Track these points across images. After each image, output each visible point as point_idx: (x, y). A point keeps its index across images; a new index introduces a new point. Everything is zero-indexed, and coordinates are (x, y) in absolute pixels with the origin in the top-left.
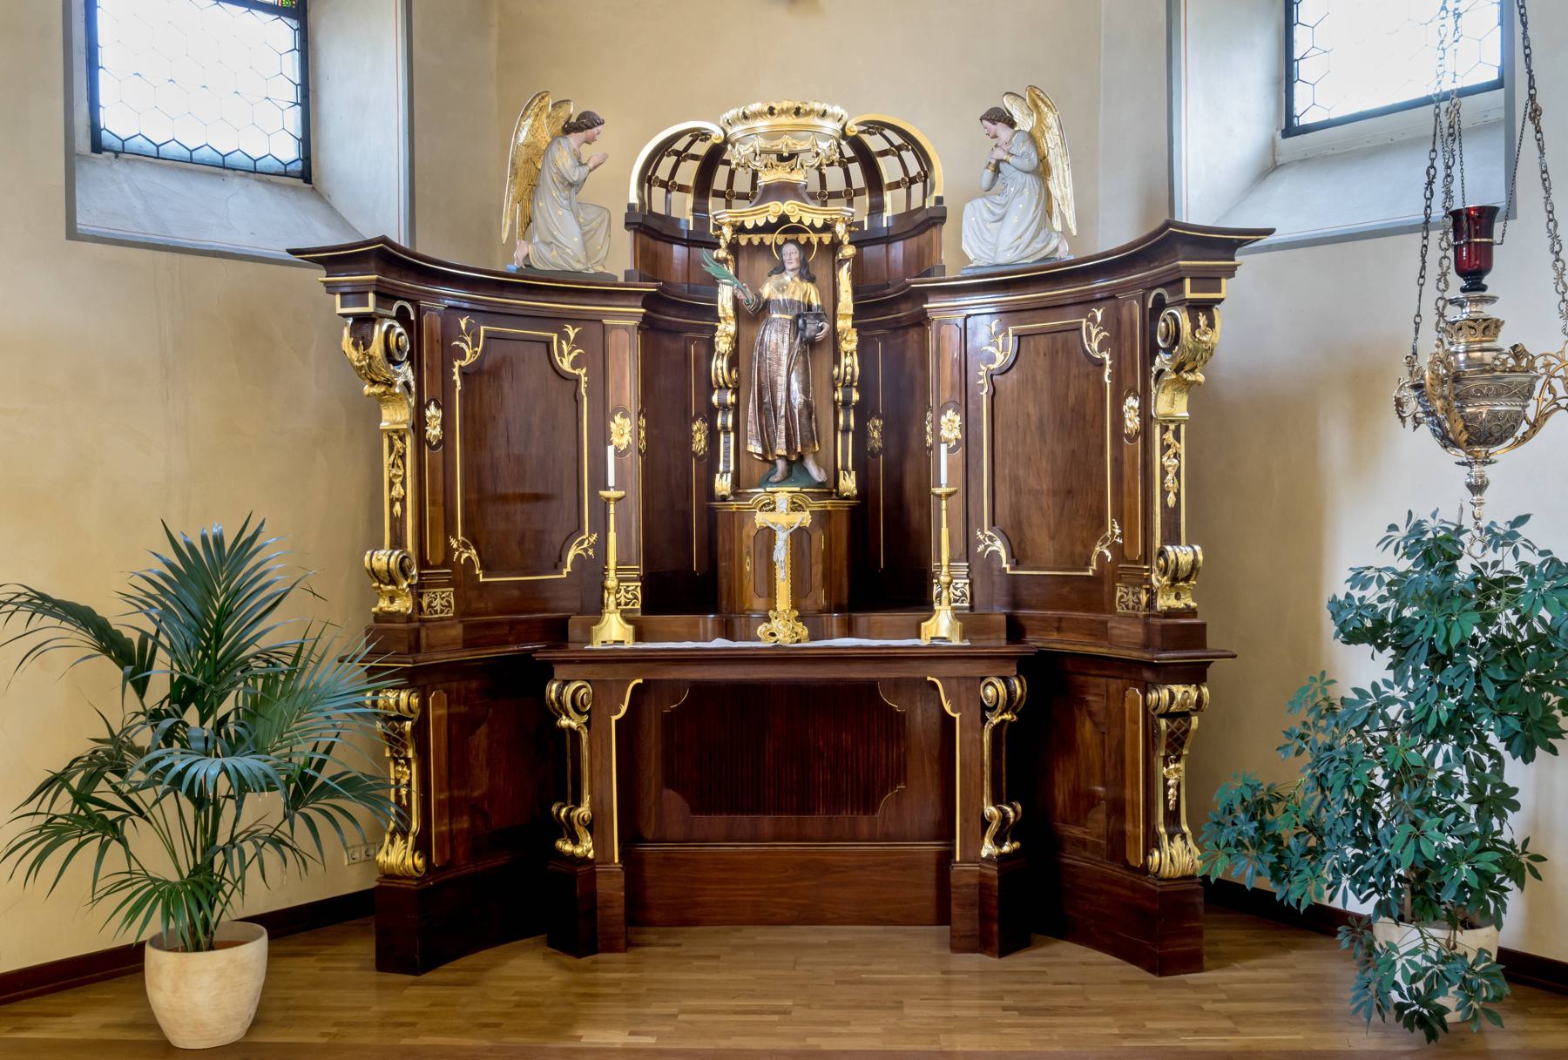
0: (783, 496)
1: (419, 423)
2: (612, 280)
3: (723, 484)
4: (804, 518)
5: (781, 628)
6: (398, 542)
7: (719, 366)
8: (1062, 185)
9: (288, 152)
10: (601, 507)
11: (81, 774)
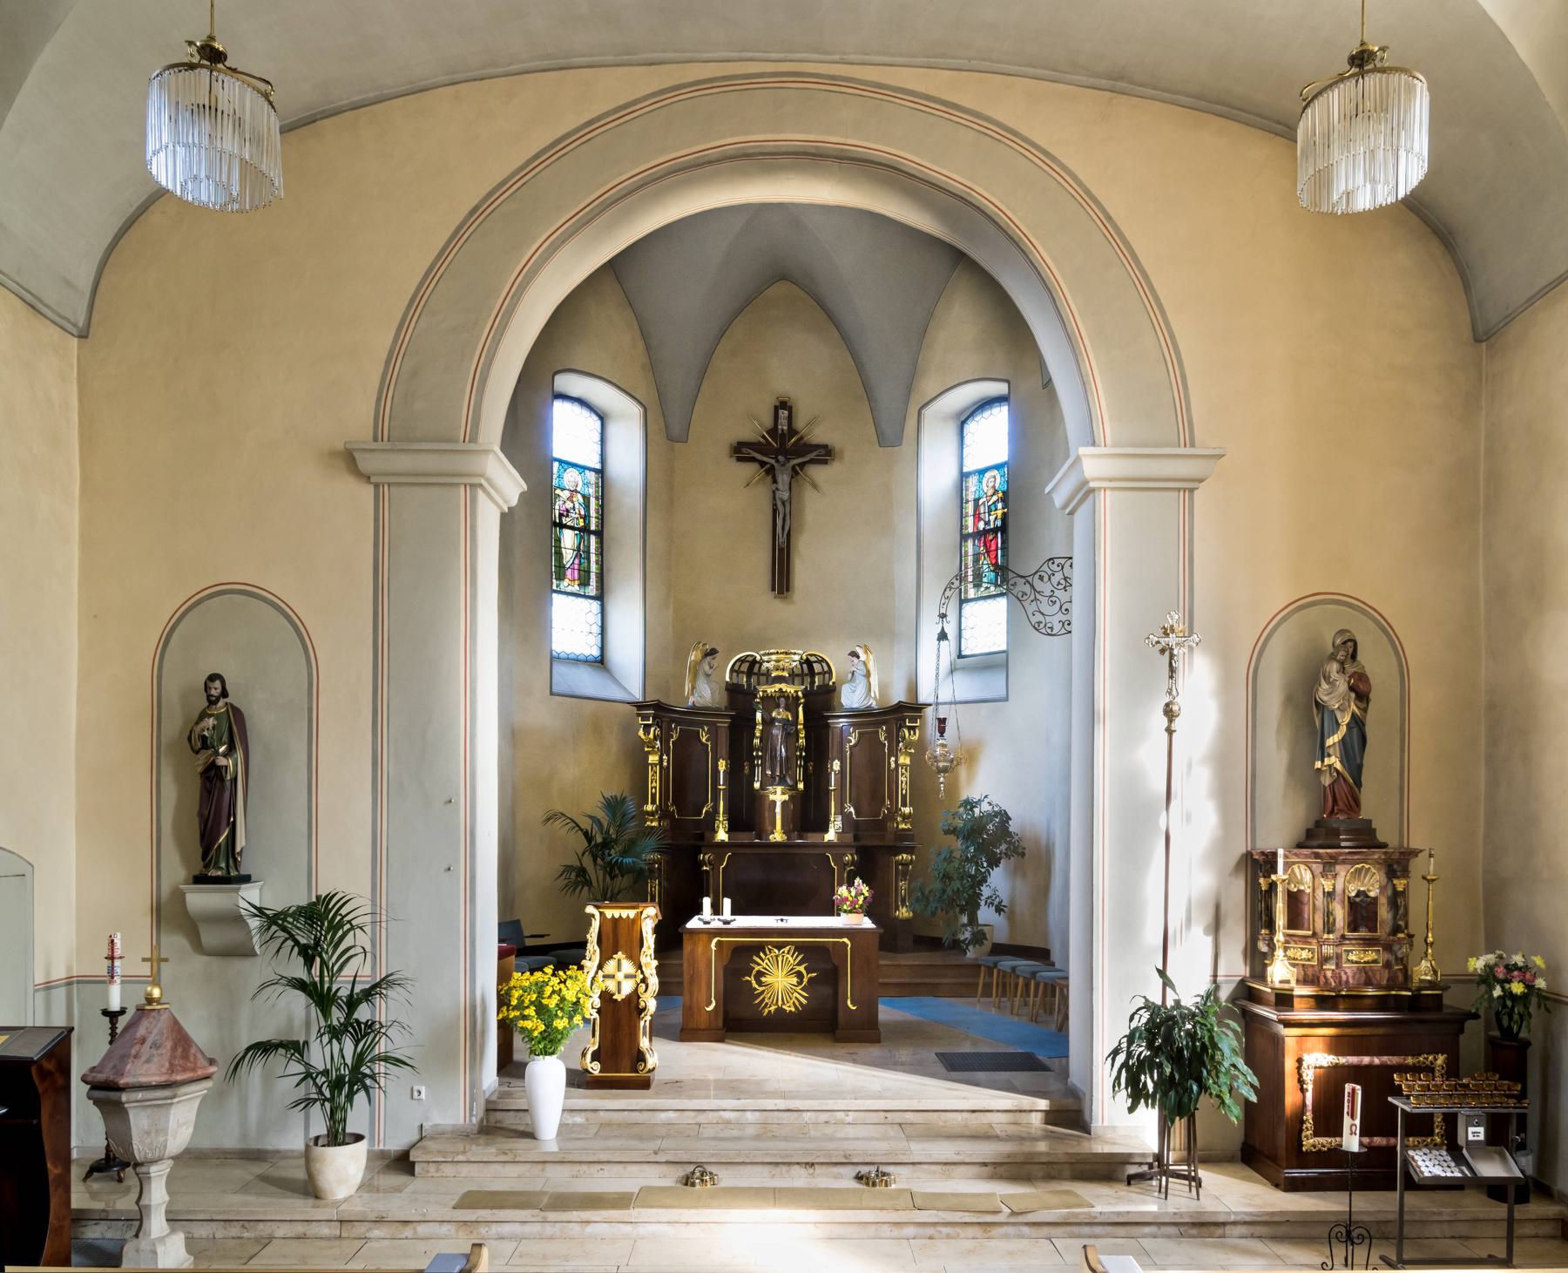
0: (779, 789)
3: (757, 785)
4: (786, 797)
5: (778, 836)
6: (653, 802)
7: (757, 741)
8: (874, 680)
9: (596, 652)
10: (716, 791)
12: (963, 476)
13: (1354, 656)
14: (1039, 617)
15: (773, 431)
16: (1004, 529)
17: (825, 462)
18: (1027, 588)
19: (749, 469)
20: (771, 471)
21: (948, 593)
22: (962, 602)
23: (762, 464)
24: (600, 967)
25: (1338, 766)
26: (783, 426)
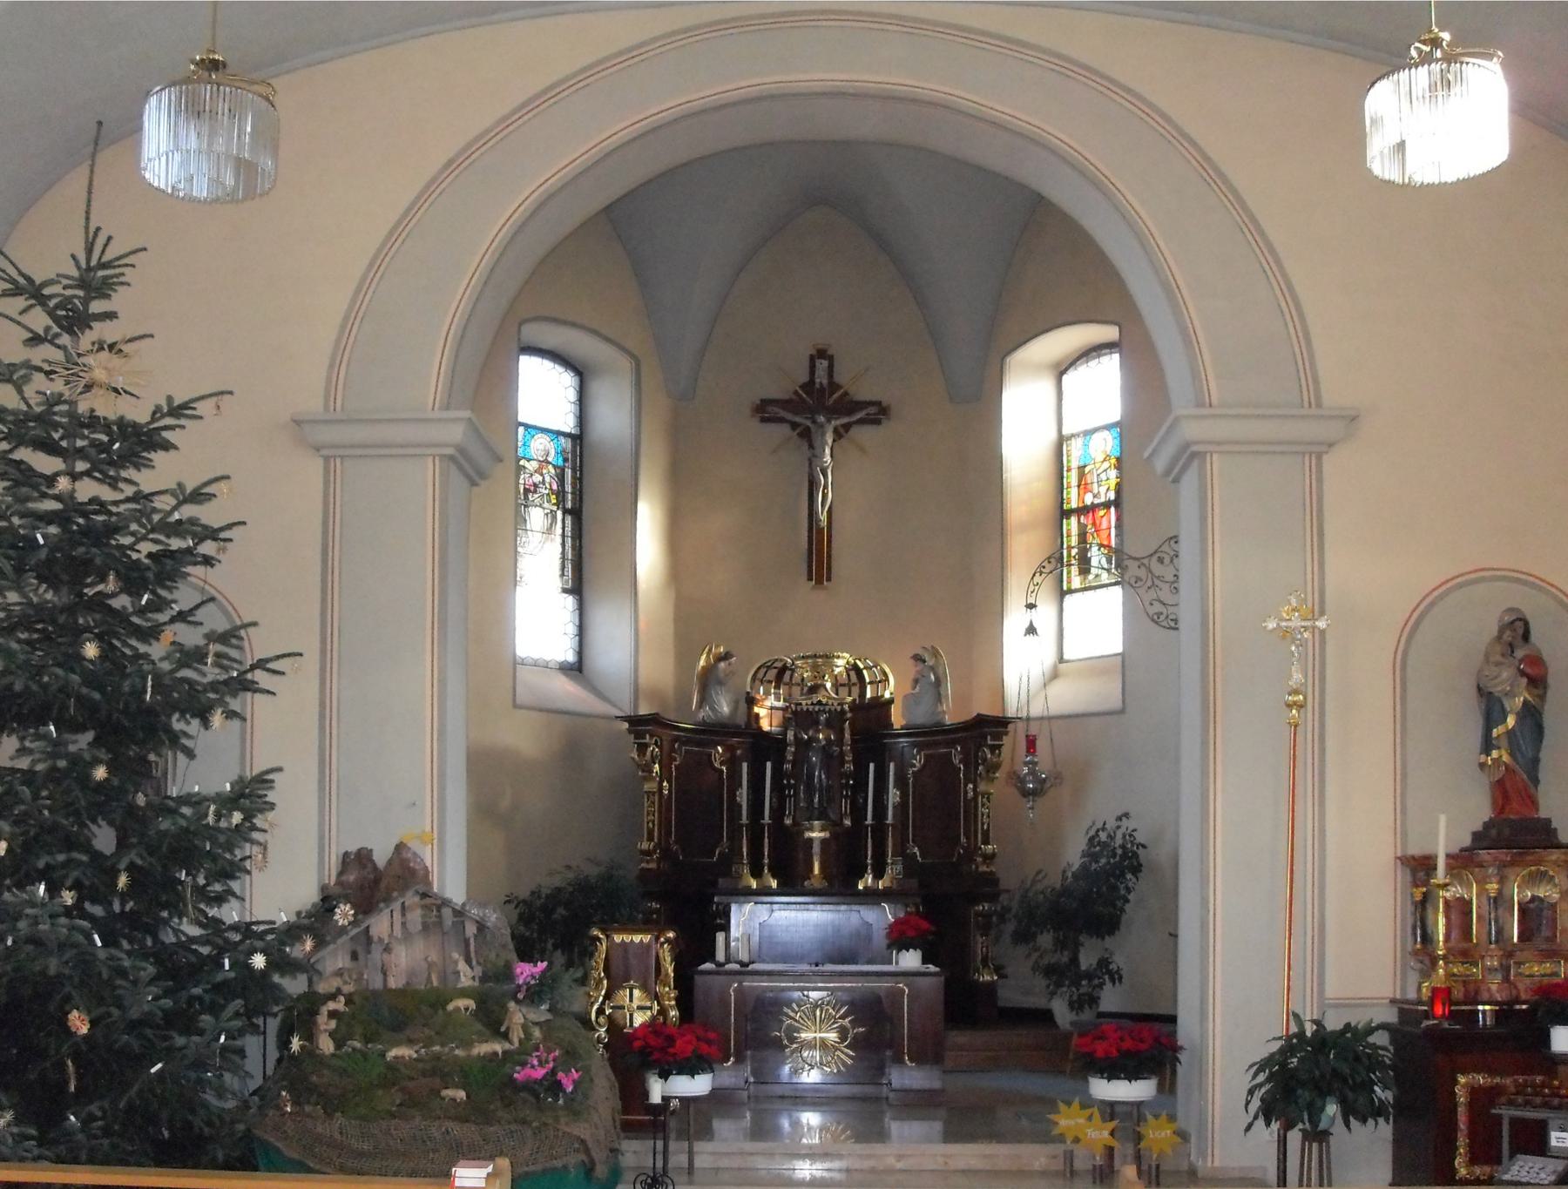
1: (661, 788)
2: (738, 727)
6: (650, 839)
7: (788, 766)
9: (570, 657)
11: (133, 642)
12: (1061, 441)
13: (1526, 636)
14: (1158, 607)
15: (808, 386)
16: (1117, 503)
17: (877, 422)
18: (1142, 573)
19: (780, 431)
20: (806, 435)
21: (1037, 579)
22: (1062, 594)
23: (794, 426)
24: (608, 997)
25: (1506, 758)
26: (821, 378)
